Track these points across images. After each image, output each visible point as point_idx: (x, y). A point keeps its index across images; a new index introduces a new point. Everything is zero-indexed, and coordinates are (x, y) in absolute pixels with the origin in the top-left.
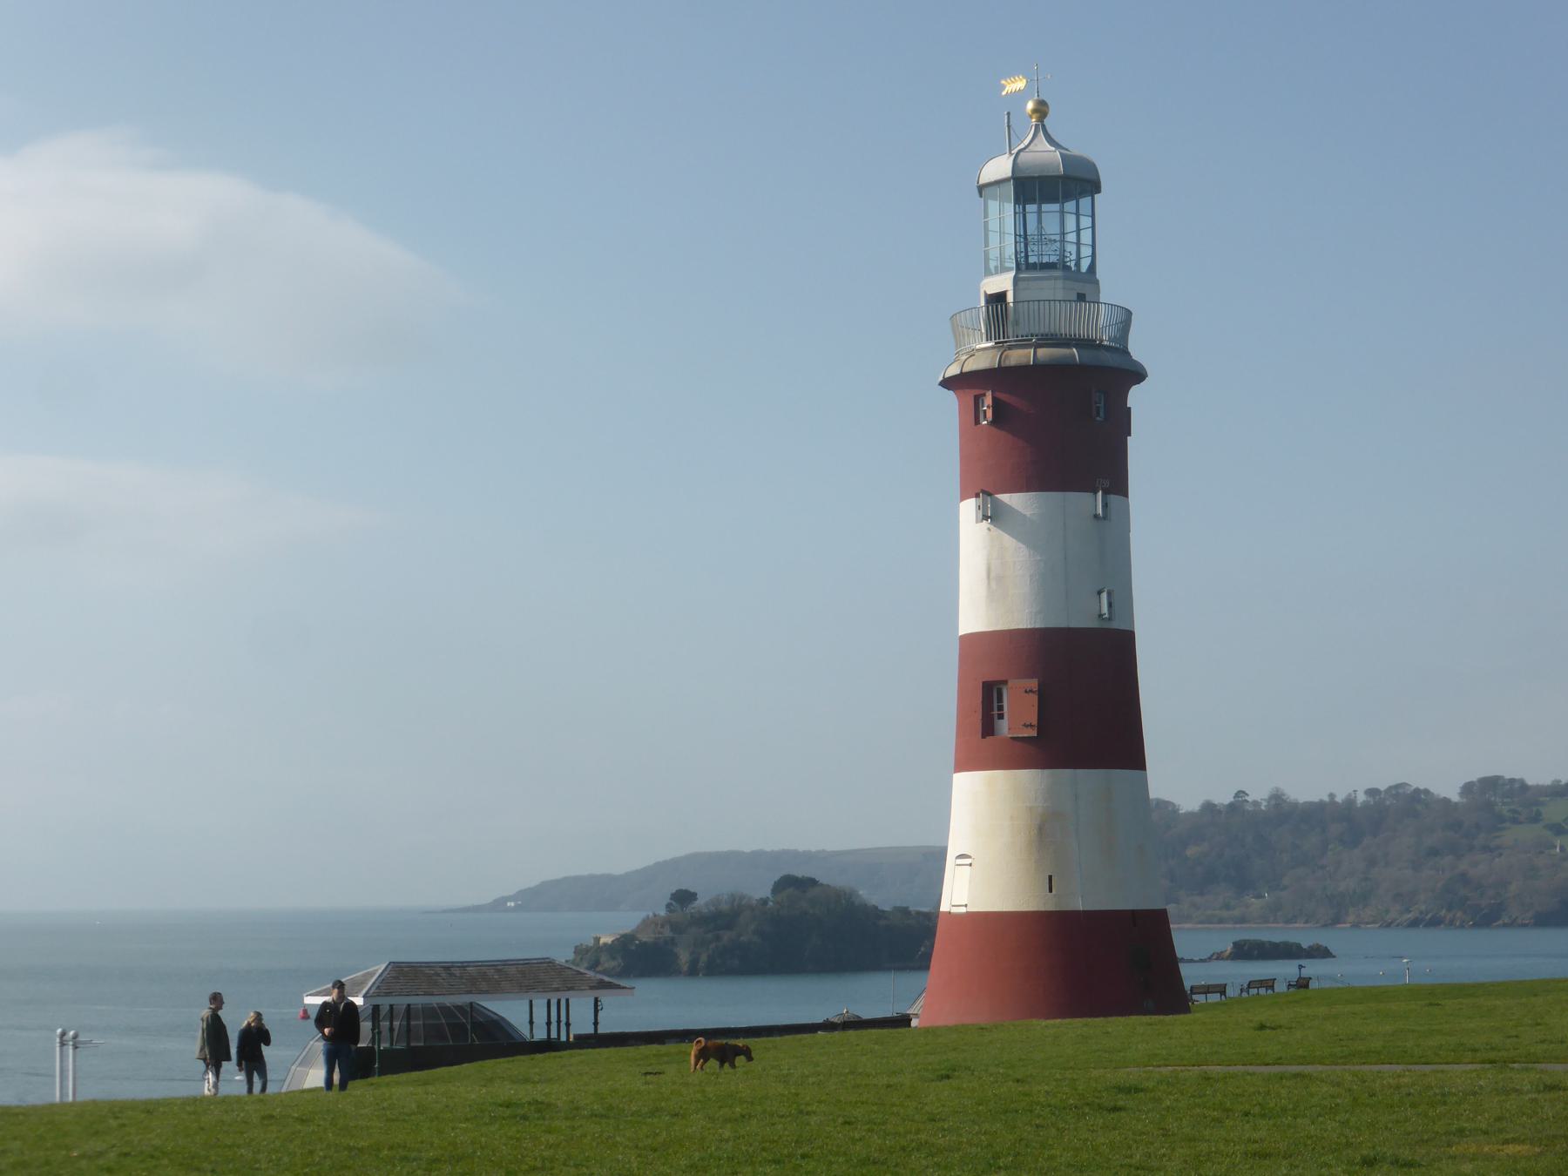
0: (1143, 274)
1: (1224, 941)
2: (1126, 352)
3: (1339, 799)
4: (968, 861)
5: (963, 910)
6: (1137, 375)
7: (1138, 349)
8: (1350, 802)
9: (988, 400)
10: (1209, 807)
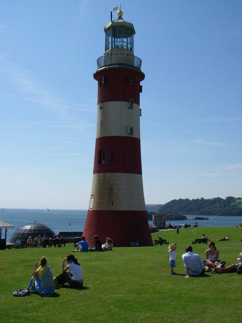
0: (143, 49)
1: (195, 216)
7: (143, 69)
8: (212, 200)
9: (103, 79)
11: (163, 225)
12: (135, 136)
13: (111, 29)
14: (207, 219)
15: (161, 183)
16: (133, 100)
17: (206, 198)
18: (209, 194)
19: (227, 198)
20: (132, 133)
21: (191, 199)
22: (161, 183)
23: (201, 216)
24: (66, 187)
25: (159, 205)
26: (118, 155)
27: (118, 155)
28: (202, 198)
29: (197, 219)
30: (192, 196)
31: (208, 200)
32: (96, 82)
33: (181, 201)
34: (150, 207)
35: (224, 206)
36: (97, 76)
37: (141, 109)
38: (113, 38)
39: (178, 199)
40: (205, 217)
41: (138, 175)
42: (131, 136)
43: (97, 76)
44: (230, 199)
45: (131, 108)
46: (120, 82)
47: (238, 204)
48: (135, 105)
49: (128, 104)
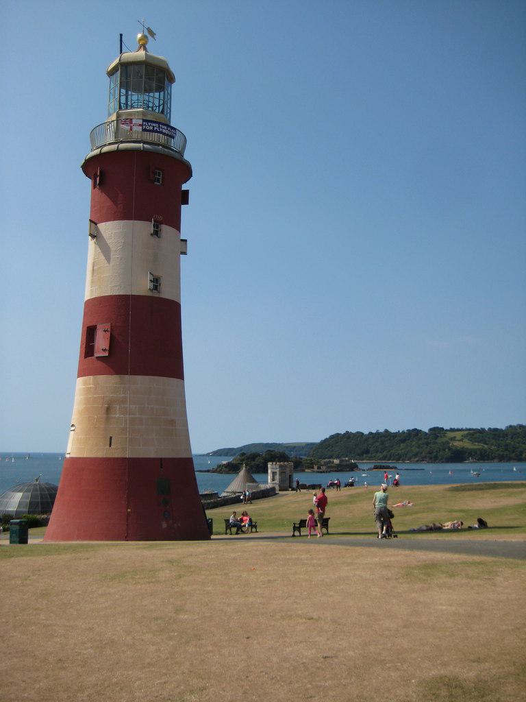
3: (401, 432)
7: (187, 156)
8: (403, 432)
10: (371, 433)
11: (288, 482)
12: (165, 293)
13: (119, 72)
15: (224, 404)
16: (161, 218)
17: (393, 430)
18: (398, 425)
19: (431, 430)
20: (156, 288)
21: (366, 432)
22: (224, 404)
23: (383, 463)
24: (57, 414)
25: (312, 444)
26: (138, 337)
27: (138, 337)
28: (386, 431)
29: (376, 467)
30: (367, 425)
31: (396, 435)
32: (86, 184)
33: (348, 435)
34: (295, 447)
35: (427, 444)
36: (89, 167)
37: (185, 241)
38: (123, 91)
39: (342, 432)
40: (391, 463)
41: (173, 381)
42: (156, 295)
43: (89, 167)
44: (437, 432)
45: (156, 233)
46: (141, 181)
48: (166, 229)
49: (148, 227)
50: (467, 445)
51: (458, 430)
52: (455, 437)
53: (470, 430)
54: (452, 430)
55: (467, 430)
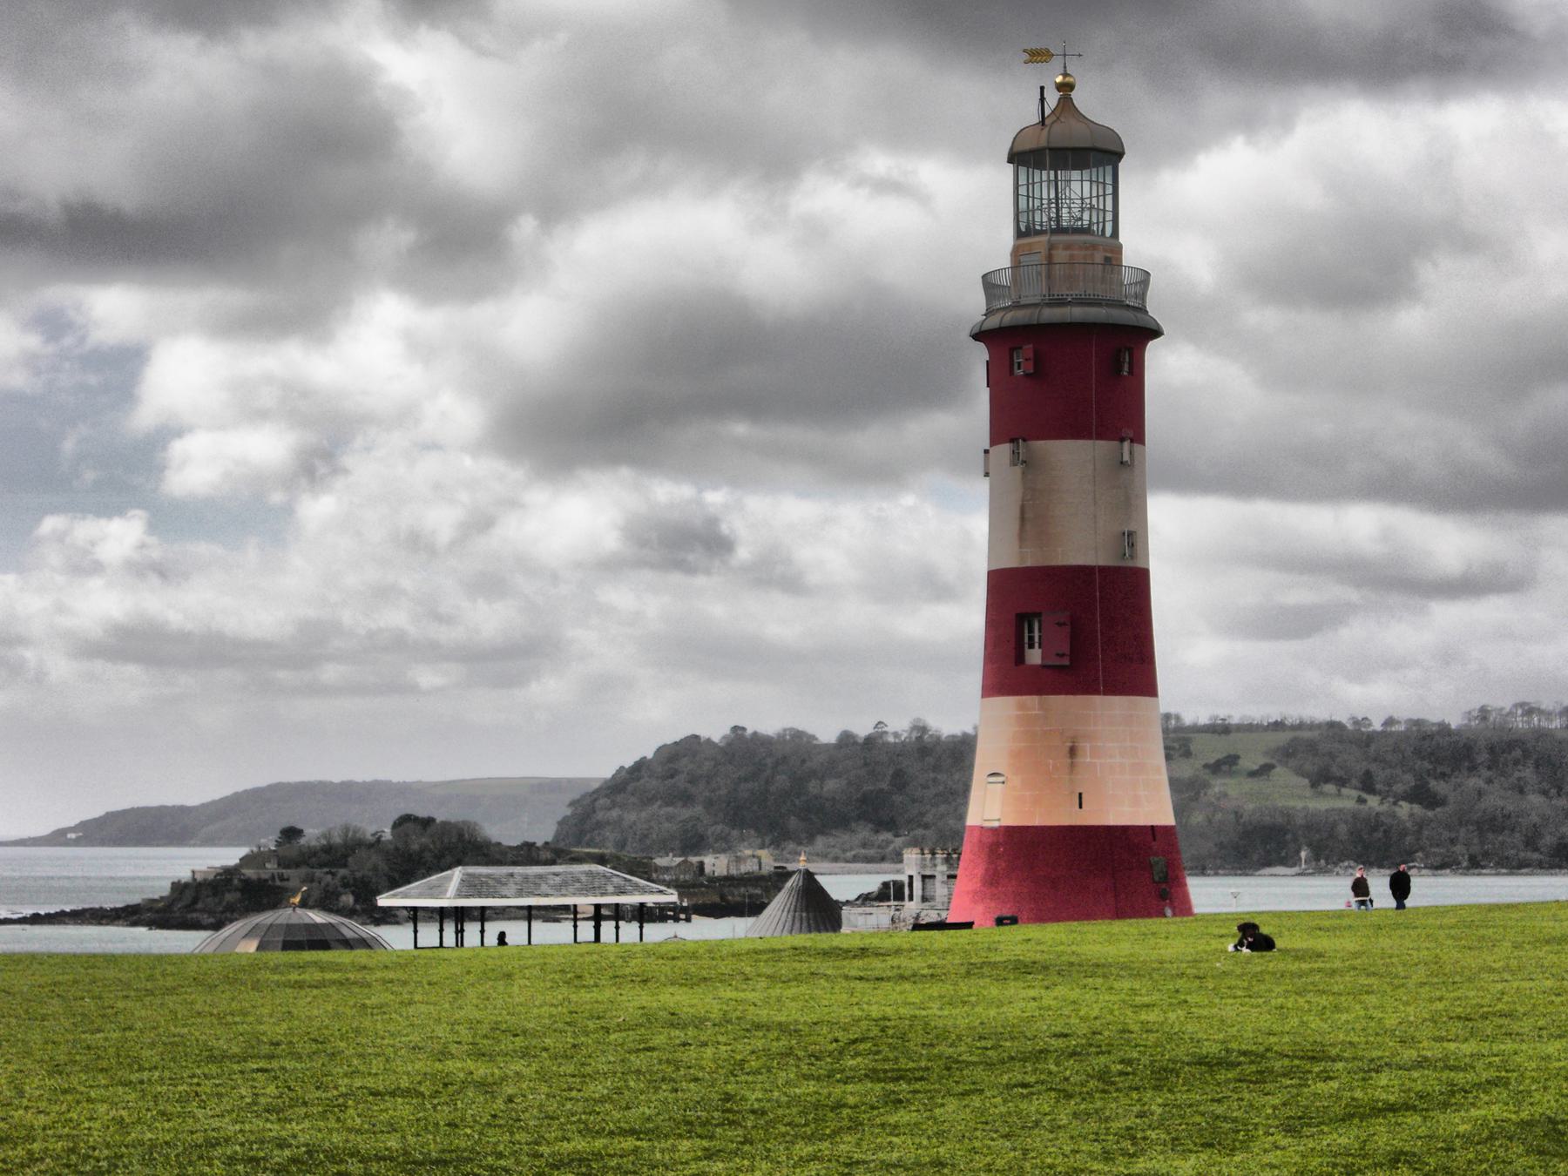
2: (1143, 310)
4: (1000, 779)
5: (996, 824)
6: (1155, 333)
7: (1156, 308)
10: (846, 739)
12: (1140, 564)
14: (364, 943)
47: (1216, 768)
48: (1137, 447)
49: (1102, 447)
50: (1291, 795)
51: (1249, 728)
52: (1232, 760)
53: (1301, 726)
54: (1221, 729)
55: (1278, 726)
